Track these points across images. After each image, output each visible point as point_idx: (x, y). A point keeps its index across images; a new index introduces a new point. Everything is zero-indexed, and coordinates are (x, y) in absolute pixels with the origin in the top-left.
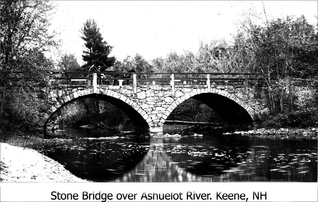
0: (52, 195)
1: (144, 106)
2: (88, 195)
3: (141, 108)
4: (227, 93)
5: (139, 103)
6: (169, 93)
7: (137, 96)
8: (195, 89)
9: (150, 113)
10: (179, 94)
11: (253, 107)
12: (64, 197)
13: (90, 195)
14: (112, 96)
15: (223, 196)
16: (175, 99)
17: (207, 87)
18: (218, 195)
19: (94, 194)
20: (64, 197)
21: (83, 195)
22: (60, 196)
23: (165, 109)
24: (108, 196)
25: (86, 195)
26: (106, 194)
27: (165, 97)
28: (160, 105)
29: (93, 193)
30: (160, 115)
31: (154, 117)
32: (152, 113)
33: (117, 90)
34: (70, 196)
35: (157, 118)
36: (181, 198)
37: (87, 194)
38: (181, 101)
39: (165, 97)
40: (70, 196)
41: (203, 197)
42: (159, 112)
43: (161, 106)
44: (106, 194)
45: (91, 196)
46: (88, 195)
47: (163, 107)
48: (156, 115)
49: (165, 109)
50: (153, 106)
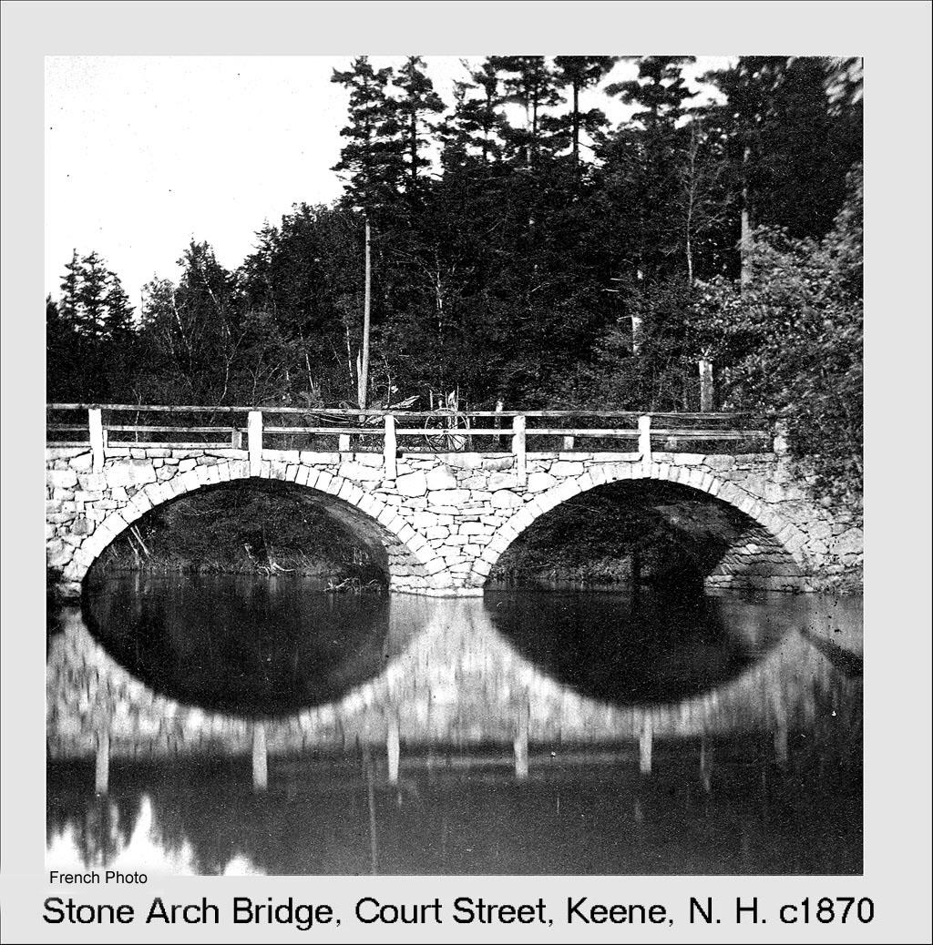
0: (457, 908)
1: (420, 520)
2: (253, 909)
3: (411, 525)
4: (709, 478)
5: (403, 511)
6: (510, 480)
7: (396, 487)
8: (599, 467)
9: (439, 543)
10: (539, 481)
11: (804, 528)
12: (86, 914)
13: (258, 908)
14: (313, 486)
15: (593, 913)
16: (527, 497)
17: (641, 459)
18: (572, 909)
19: (270, 907)
20: (86, 914)
21: (236, 909)
22: (485, 911)
23: (492, 529)
24: (318, 913)
25: (247, 909)
26: (310, 908)
27: (493, 493)
28: (476, 518)
29: (268, 903)
30: (475, 550)
31: (453, 556)
32: (447, 542)
33: (331, 467)
34: (106, 912)
35: (463, 559)
36: (440, 919)
37: (250, 904)
38: (546, 504)
39: (493, 493)
40: (106, 912)
41: (523, 916)
42: (473, 539)
43: (479, 521)
44: (310, 908)
45: (261, 911)
46: (253, 909)
47: (485, 524)
48: (461, 550)
49: (490, 530)
50: (449, 520)
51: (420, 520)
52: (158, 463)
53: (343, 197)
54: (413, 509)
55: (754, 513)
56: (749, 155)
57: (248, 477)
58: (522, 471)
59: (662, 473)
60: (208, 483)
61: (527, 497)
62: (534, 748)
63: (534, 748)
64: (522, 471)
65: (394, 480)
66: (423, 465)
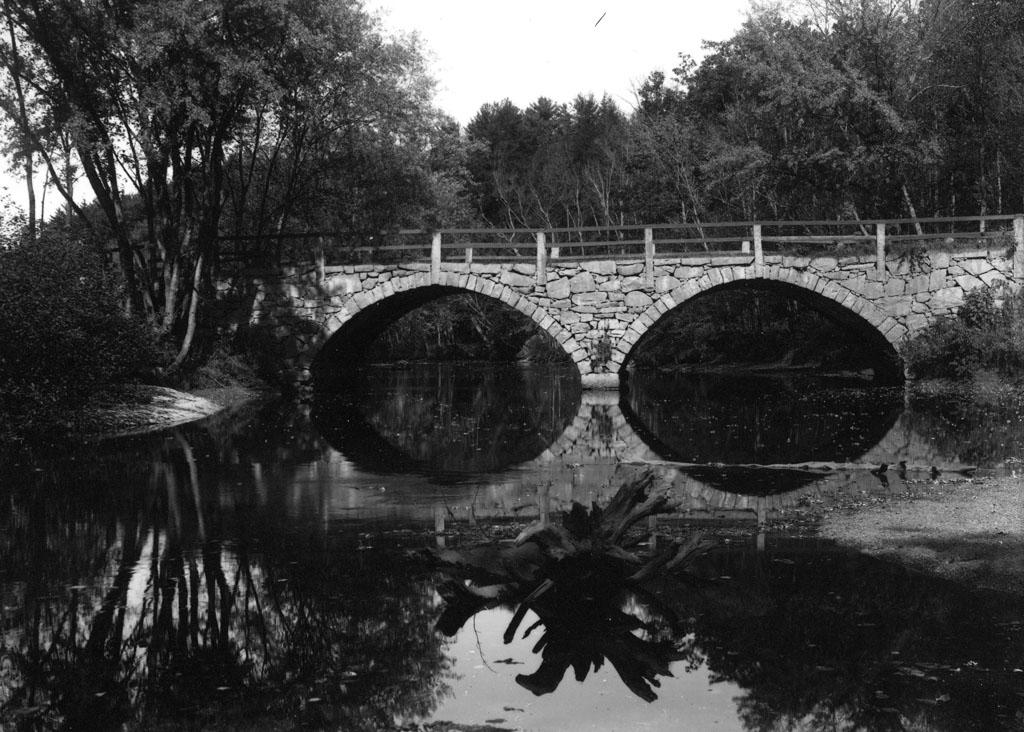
10: (665, 283)
28: (612, 315)
43: (614, 317)
47: (619, 321)
50: (590, 318)
51: (570, 319)
52: (363, 275)
53: (591, 103)
54: (560, 309)
55: (857, 307)
56: (732, 651)
57: (429, 284)
58: (651, 274)
59: (773, 273)
60: (401, 290)
61: (655, 297)
62: (868, 248)
63: (868, 248)
64: (651, 274)
65: (544, 286)
66: (567, 272)
